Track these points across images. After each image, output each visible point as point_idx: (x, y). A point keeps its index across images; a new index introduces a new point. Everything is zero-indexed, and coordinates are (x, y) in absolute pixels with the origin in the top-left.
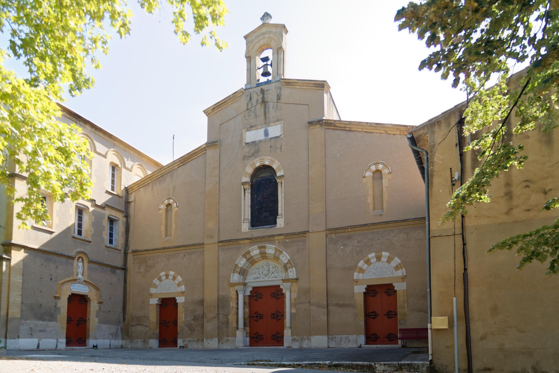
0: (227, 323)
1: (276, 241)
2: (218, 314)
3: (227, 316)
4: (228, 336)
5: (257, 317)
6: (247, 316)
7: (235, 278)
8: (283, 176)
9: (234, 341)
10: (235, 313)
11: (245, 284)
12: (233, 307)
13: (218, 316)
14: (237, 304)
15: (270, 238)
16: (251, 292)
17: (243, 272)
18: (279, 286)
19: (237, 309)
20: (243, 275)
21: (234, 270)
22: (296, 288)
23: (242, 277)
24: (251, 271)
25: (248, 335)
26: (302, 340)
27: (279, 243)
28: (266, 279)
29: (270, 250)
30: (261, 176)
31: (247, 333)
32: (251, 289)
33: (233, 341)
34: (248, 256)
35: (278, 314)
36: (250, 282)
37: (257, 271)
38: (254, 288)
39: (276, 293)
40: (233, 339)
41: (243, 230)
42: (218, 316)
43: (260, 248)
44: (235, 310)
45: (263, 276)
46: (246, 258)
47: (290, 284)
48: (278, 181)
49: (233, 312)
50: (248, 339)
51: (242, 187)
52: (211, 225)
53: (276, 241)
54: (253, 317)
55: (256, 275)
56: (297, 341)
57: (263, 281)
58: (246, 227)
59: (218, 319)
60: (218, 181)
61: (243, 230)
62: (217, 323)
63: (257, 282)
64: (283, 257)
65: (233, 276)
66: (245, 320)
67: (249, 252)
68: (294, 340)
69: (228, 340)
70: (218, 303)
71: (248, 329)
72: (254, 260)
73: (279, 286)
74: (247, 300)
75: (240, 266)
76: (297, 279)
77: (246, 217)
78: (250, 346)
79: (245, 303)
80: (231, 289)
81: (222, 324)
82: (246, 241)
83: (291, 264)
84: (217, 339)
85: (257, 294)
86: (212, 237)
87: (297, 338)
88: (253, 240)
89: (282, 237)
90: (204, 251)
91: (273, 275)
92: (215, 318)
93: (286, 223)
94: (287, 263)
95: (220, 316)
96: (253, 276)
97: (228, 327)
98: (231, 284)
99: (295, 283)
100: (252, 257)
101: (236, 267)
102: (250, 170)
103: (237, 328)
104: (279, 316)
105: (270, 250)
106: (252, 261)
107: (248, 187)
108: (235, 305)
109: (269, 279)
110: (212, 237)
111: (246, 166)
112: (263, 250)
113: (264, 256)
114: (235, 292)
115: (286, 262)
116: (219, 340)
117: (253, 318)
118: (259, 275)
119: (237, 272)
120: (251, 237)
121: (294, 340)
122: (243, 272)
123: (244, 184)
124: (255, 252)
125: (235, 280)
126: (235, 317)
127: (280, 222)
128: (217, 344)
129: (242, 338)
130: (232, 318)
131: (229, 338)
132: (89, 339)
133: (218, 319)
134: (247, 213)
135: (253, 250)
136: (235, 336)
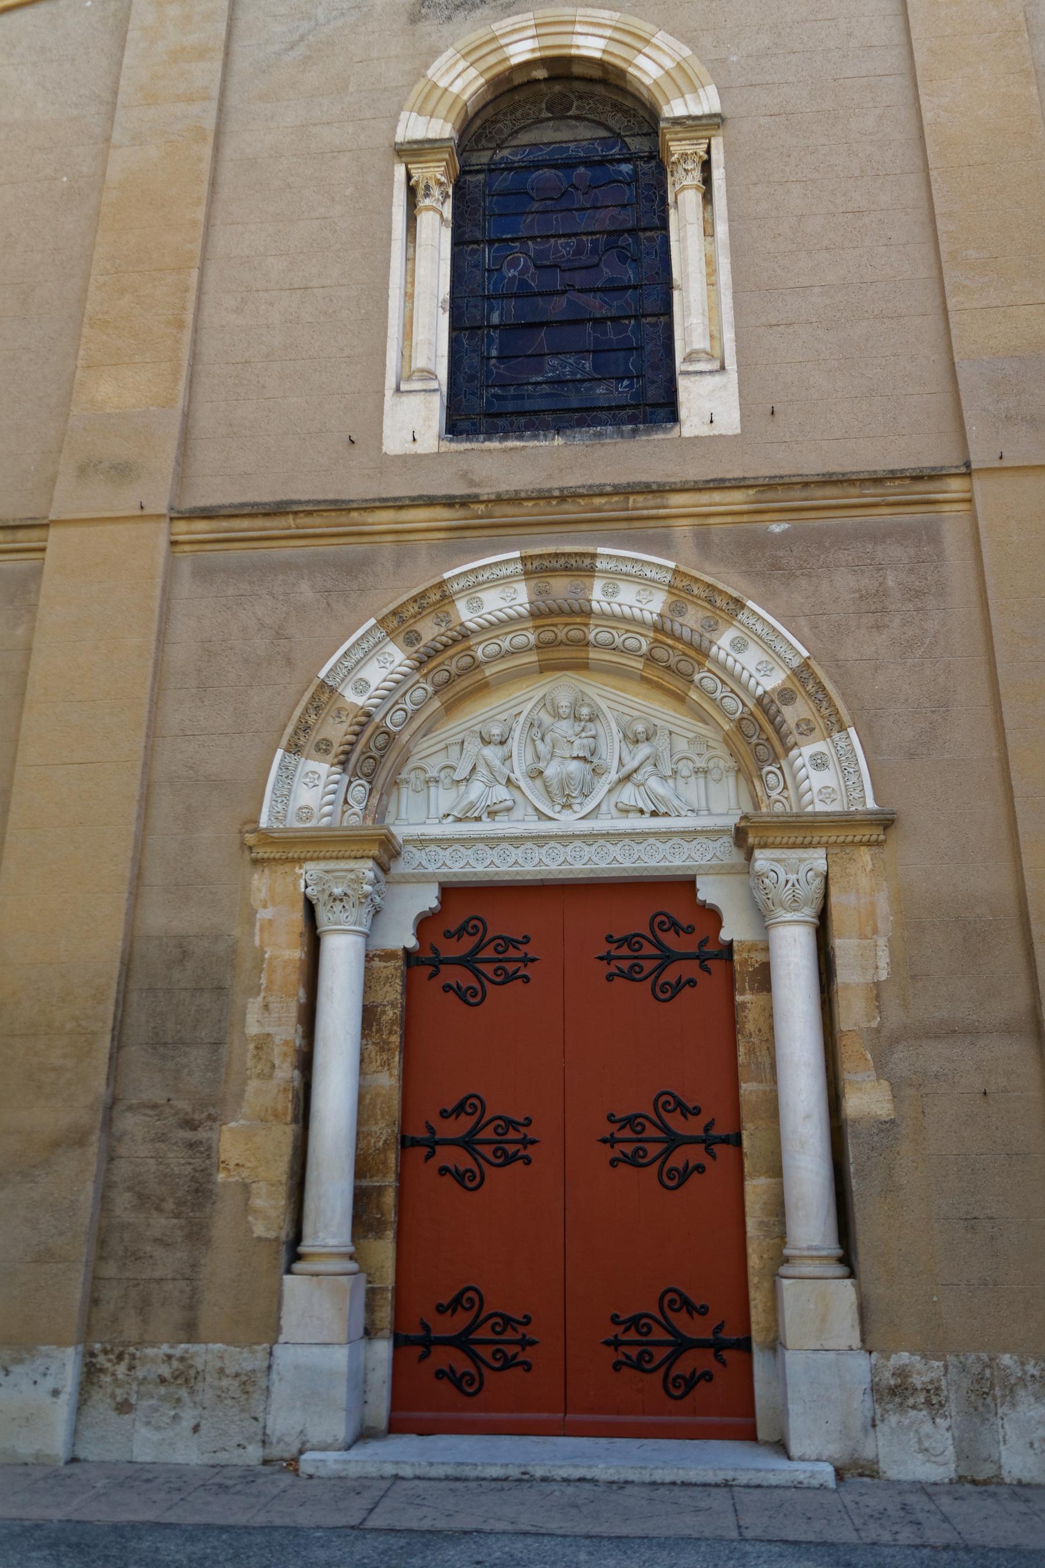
0: (201, 1191)
1: (682, 529)
2: (111, 1107)
3: (195, 1125)
4: (190, 1331)
5: (468, 1143)
6: (384, 1130)
7: (309, 792)
8: (715, 122)
9: (252, 1386)
10: (286, 1105)
11: (387, 852)
12: (263, 1043)
13: (108, 1122)
14: (309, 1016)
15: (632, 510)
16: (424, 924)
17: (373, 755)
18: (687, 884)
19: (306, 1062)
20: (370, 777)
21: (304, 728)
22: (883, 905)
23: (359, 791)
24: (429, 754)
25: (385, 1314)
26: (986, 1394)
27: (704, 542)
28: (568, 821)
29: (628, 593)
30: (524, 138)
31: (372, 1294)
32: (429, 899)
33: (247, 1382)
34: (429, 631)
35: (676, 1122)
36: (422, 842)
37: (491, 753)
38: (449, 891)
39: (661, 942)
40: (249, 1360)
41: (395, 441)
42: (108, 1122)
43: (536, 569)
44: (286, 1072)
45: (560, 791)
46: (412, 639)
47: (817, 859)
48: (677, 148)
49: (267, 1090)
50: (383, 1349)
51: (400, 171)
52: (123, 391)
53: (682, 529)
54: (432, 1144)
55: (476, 790)
56: (933, 1402)
57: (541, 840)
58: (413, 422)
59: (110, 1157)
60: (209, 123)
61: (395, 441)
62: (88, 1194)
63: (492, 841)
64: (739, 646)
65: (287, 774)
66: (363, 1165)
67: (438, 599)
68: (893, 1393)
69: (186, 1376)
70: (122, 1001)
71: (384, 1251)
72: (476, 665)
73: (687, 884)
74: (392, 993)
75: (352, 697)
76: (885, 822)
77: (420, 362)
78: (396, 1427)
79: (369, 1016)
80: (260, 883)
81: (143, 1200)
82: (420, 516)
83: (820, 695)
84: (66, 1365)
85: (473, 946)
86: (122, 472)
87: (924, 1372)
88: (475, 517)
89: (737, 499)
90: (37, 573)
91: (629, 795)
92: (78, 1139)
93: (759, 407)
94: (786, 695)
95: (129, 1123)
96: (444, 799)
97: (198, 1235)
98: (267, 838)
99: (865, 856)
100: (465, 635)
101: (316, 706)
102: (460, 80)
103: (293, 1250)
104: (698, 1136)
105: (628, 593)
106: (453, 673)
107: (434, 172)
108: (289, 1032)
109: (586, 826)
110: (122, 472)
111: (435, 53)
112: (560, 587)
113: (562, 639)
114: (298, 915)
115: (772, 681)
116: (91, 1372)
117: (437, 1146)
118: (501, 793)
119: (323, 748)
120: (459, 489)
121: (893, 1393)
122: (373, 755)
123: (411, 152)
124: (495, 598)
125: (305, 812)
126: (285, 1134)
127: (709, 403)
128: (62, 1411)
129: (339, 1357)
130: (246, 1148)
131: (205, 1353)
132: (300, 959)
133: (110, 1157)
134: (425, 334)
135: (477, 583)
136: (269, 1329)
